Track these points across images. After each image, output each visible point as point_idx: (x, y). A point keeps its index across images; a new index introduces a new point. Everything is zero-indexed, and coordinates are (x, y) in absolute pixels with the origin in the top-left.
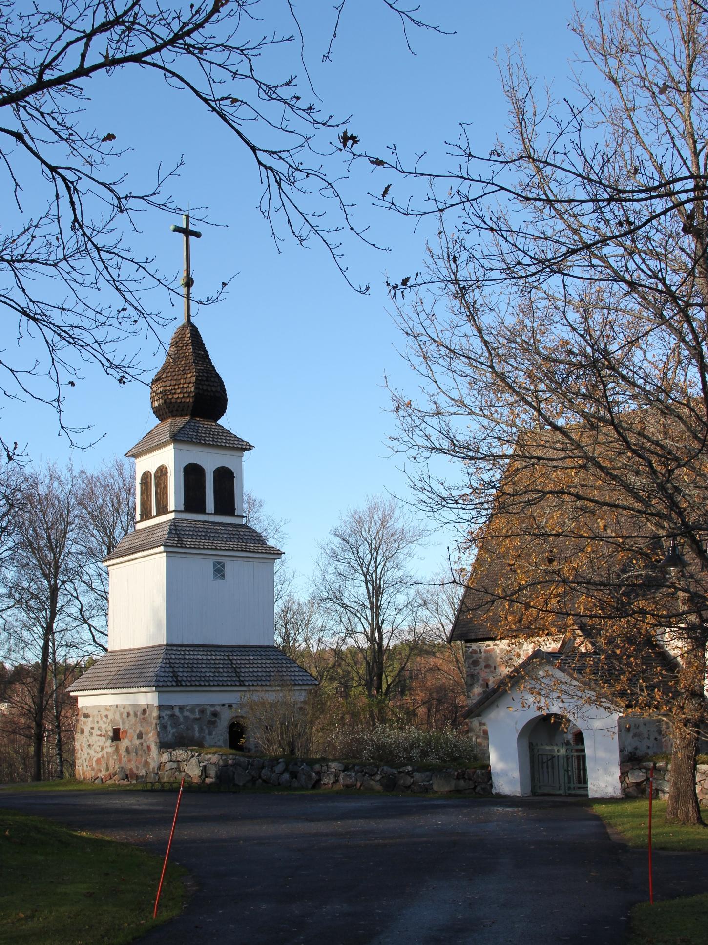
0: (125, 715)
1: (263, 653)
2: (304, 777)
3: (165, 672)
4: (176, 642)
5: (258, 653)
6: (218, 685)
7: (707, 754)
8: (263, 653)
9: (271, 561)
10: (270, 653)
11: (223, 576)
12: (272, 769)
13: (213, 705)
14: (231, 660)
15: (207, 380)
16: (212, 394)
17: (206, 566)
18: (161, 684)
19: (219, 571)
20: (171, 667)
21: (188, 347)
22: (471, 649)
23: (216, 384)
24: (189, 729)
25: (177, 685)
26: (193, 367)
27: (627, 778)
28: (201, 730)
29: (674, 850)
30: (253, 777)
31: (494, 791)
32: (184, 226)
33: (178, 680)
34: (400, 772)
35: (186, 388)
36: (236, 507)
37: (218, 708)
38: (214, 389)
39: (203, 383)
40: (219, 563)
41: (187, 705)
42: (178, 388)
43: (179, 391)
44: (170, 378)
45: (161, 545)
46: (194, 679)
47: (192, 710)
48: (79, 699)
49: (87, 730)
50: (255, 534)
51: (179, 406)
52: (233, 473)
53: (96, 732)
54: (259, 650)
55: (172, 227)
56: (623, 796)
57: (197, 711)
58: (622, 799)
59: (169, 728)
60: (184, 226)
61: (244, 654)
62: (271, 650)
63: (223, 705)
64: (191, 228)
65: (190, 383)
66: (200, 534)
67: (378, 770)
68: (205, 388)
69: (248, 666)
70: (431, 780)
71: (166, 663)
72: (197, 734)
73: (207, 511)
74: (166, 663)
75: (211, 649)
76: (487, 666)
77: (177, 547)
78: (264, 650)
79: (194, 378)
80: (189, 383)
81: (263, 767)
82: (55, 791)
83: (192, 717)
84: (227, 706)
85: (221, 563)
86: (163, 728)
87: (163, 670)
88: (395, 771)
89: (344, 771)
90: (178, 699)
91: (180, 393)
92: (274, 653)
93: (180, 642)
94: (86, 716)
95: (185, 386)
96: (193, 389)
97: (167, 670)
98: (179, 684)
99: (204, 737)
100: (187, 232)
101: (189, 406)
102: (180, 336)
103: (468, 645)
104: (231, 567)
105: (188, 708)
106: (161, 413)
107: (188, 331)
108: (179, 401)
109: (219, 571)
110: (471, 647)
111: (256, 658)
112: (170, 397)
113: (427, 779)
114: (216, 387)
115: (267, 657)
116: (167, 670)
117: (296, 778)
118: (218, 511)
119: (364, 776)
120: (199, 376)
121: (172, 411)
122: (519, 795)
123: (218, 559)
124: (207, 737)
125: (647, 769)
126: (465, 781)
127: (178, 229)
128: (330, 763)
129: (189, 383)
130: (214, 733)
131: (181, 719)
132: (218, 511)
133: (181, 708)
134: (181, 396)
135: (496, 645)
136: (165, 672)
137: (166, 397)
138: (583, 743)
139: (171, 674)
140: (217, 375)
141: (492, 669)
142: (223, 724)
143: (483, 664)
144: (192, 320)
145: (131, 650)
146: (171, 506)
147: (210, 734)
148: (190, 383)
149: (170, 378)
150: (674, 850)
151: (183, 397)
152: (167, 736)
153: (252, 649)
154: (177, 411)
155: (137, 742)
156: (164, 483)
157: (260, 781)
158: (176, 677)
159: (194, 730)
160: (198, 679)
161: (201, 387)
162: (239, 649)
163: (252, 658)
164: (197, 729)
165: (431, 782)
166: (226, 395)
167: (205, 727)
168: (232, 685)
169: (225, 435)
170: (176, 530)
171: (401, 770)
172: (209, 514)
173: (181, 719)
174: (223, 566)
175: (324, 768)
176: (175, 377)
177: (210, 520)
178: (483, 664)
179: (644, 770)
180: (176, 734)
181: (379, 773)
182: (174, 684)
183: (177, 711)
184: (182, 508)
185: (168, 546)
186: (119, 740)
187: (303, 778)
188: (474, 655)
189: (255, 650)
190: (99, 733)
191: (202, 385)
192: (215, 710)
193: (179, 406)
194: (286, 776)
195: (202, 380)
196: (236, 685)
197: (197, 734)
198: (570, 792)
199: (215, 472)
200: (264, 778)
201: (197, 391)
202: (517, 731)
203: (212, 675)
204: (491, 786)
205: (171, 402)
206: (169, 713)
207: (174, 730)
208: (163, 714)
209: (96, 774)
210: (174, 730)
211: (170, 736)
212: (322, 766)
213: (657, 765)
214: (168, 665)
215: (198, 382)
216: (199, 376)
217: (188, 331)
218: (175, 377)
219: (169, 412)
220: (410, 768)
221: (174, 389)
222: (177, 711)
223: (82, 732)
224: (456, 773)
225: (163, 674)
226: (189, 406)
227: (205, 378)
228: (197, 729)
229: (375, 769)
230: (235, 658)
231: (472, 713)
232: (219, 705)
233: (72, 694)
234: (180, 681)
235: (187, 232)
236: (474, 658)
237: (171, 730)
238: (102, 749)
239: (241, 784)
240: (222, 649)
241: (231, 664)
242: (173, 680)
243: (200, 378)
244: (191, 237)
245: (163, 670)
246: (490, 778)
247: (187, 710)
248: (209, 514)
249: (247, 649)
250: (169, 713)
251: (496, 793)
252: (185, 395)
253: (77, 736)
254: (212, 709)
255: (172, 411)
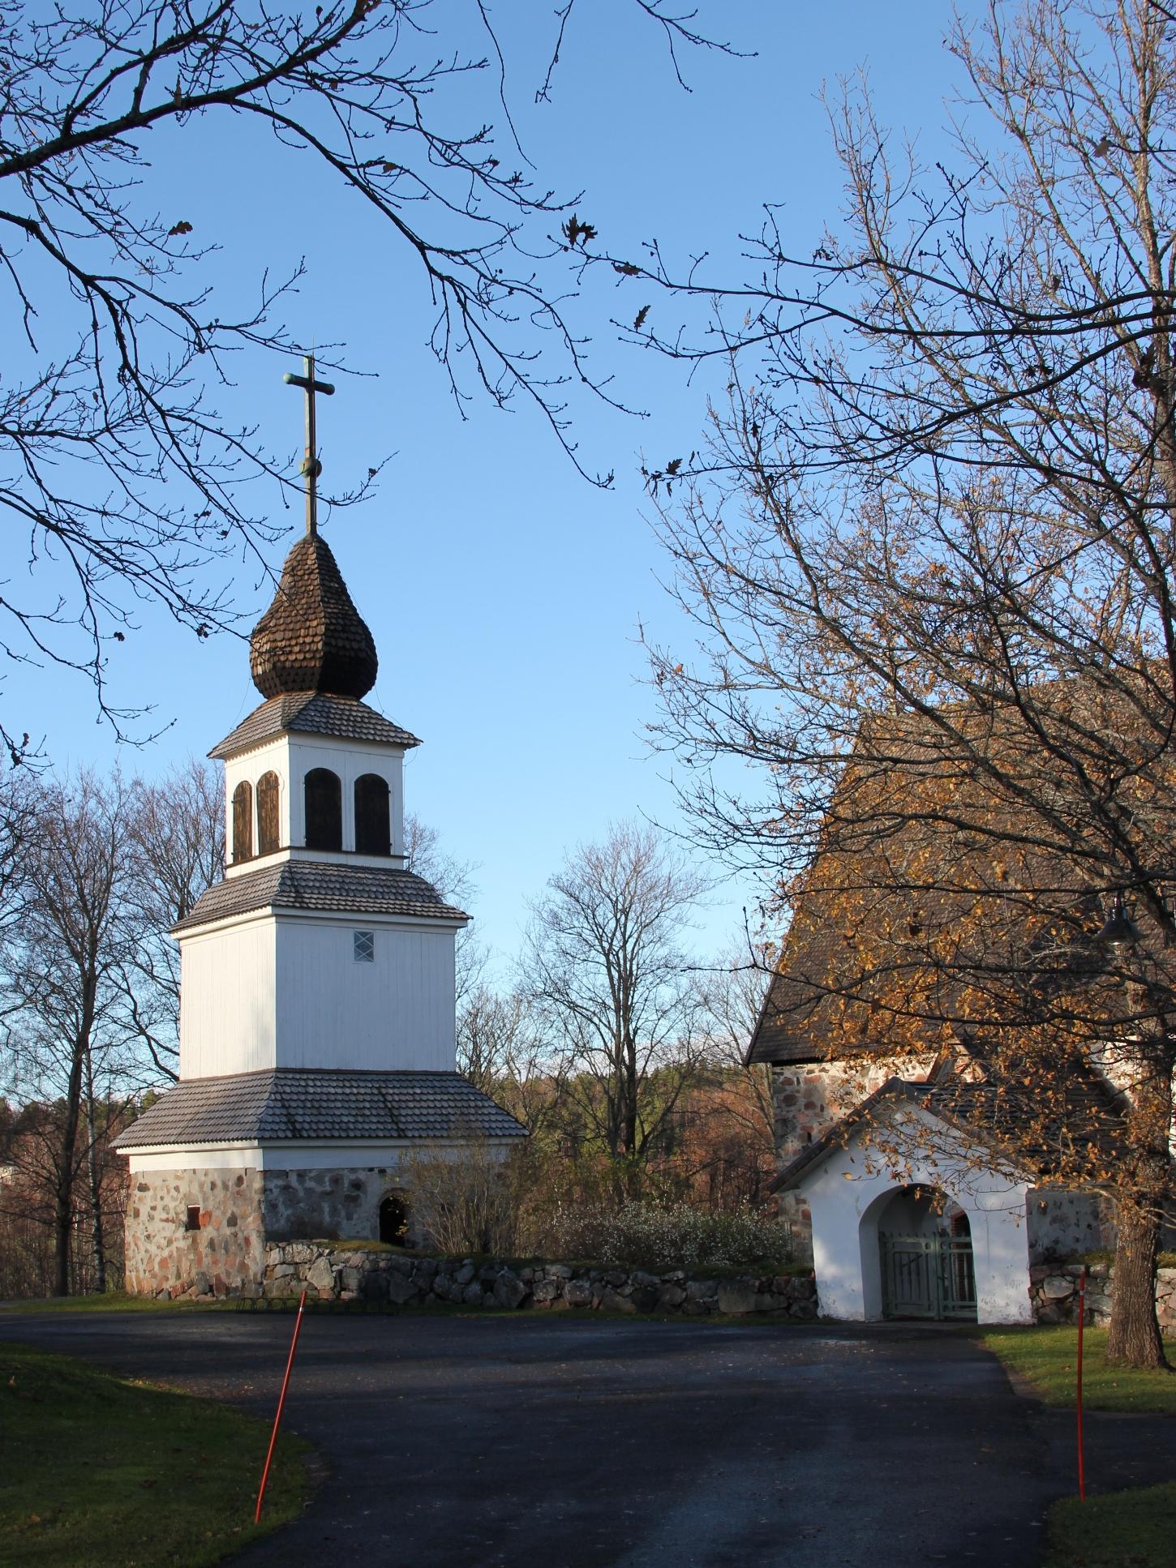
0: (207, 1187)
1: (437, 1084)
2: (505, 1289)
3: (274, 1114)
4: (292, 1065)
5: (429, 1084)
6: (363, 1137)
7: (1174, 1251)
8: (437, 1084)
9: (451, 931)
10: (449, 1083)
11: (371, 955)
12: (452, 1275)
13: (353, 1170)
14: (383, 1095)
15: (343, 631)
16: (353, 654)
17: (343, 939)
18: (267, 1135)
19: (364, 948)
20: (283, 1107)
21: (312, 577)
22: (782, 1078)
23: (358, 638)
24: (314, 1210)
25: (294, 1137)
26: (321, 608)
27: (1041, 1291)
28: (334, 1211)
29: (1119, 1411)
30: (421, 1290)
31: (820, 1313)
32: (306, 375)
33: (295, 1129)
34: (664, 1282)
35: (310, 644)
36: (392, 841)
37: (362, 1176)
38: (355, 645)
39: (336, 635)
40: (364, 934)
41: (310, 1171)
42: (296, 644)
43: (297, 649)
44: (282, 628)
45: (268, 904)
46: (322, 1126)
47: (319, 1179)
48: (132, 1159)
49: (144, 1211)
50: (423, 886)
51: (297, 674)
52: (386, 785)
53: (160, 1214)
54: (431, 1078)
55: (286, 377)
56: (1035, 1321)
57: (327, 1179)
58: (1033, 1325)
59: (281, 1208)
60: (306, 375)
61: (405, 1084)
62: (451, 1078)
63: (371, 1170)
64: (318, 378)
65: (315, 635)
66: (332, 886)
67: (628, 1278)
68: (340, 643)
69: (411, 1105)
70: (716, 1294)
71: (276, 1100)
72: (327, 1218)
73: (344, 848)
74: (276, 1100)
75: (350, 1077)
76: (810, 1105)
77: (294, 907)
78: (438, 1078)
79: (323, 627)
80: (314, 636)
81: (437, 1273)
82: (91, 1313)
83: (319, 1189)
84: (376, 1171)
85: (367, 934)
86: (270, 1207)
87: (271, 1112)
88: (656, 1280)
89: (571, 1279)
90: (296, 1160)
91: (300, 652)
92: (455, 1083)
93: (299, 1066)
94: (143, 1188)
95: (308, 640)
96: (320, 646)
97: (278, 1111)
98: (297, 1134)
99: (338, 1224)
100: (311, 386)
101: (313, 674)
102: (299, 558)
103: (778, 1069)
104: (384, 941)
105: (312, 1175)
106: (267, 685)
107: (311, 550)
108: (297, 665)
109: (364, 948)
110: (782, 1074)
111: (425, 1091)
112: (282, 658)
113: (709, 1293)
114: (359, 642)
115: (444, 1090)
116: (278, 1111)
117: (492, 1290)
118: (363, 848)
119: (605, 1287)
120: (331, 623)
121: (286, 683)
122: (863, 1319)
123: (363, 928)
124: (344, 1222)
125: (1075, 1276)
126: (772, 1297)
127: (295, 381)
128: (547, 1267)
129: (314, 636)
130: (355, 1216)
131: (301, 1194)
132: (363, 848)
133: (301, 1175)
134: (301, 657)
135: (823, 1070)
136: (274, 1114)
137: (276, 659)
138: (968, 1233)
139: (284, 1119)
140: (361, 622)
141: (818, 1110)
142: (371, 1201)
143: (802, 1102)
144: (320, 531)
145: (218, 1079)
146: (285, 840)
147: (349, 1217)
148: (315, 635)
149: (282, 628)
150: (1119, 1411)
151: (305, 658)
152: (278, 1221)
153: (419, 1077)
154: (294, 681)
155: (228, 1231)
156: (272, 801)
157: (432, 1295)
158: (293, 1123)
159: (322, 1212)
160: (329, 1126)
161: (333, 643)
162: (397, 1078)
163: (418, 1091)
164: (327, 1209)
165: (716, 1298)
166: (375, 656)
167: (340, 1206)
168: (385, 1137)
169: (373, 721)
170: (292, 879)
171: (666, 1278)
172: (347, 853)
173: (301, 1194)
174: (371, 940)
175: (537, 1274)
176: (291, 626)
177: (350, 863)
178: (802, 1102)
179: (1069, 1278)
180: (293, 1219)
181: (630, 1282)
182: (289, 1134)
183: (293, 1180)
184: (302, 842)
185: (280, 906)
186: (198, 1228)
187: (503, 1291)
188: (787, 1087)
189: (424, 1078)
190: (164, 1216)
191: (336, 639)
192: (357, 1178)
193: (297, 674)
194: (476, 1288)
195: (335, 630)
196: (392, 1137)
197: (327, 1218)
198: (947, 1314)
199: (357, 783)
200: (439, 1290)
201: (328, 649)
202: (859, 1212)
203: (352, 1119)
204: (816, 1304)
205: (284, 668)
206: (280, 1182)
207: (289, 1212)
208: (271, 1185)
209: (160, 1284)
210: (289, 1212)
211: (283, 1221)
212: (535, 1271)
213: (1092, 1269)
214: (279, 1104)
215: (330, 634)
216: (331, 623)
217: (311, 550)
218: (291, 626)
219: (281, 684)
220: (680, 1274)
221: (290, 646)
222: (293, 1180)
223: (137, 1214)
224: (757, 1283)
225: (270, 1119)
226: (313, 674)
227: (340, 628)
228: (327, 1209)
229: (624, 1277)
230: (391, 1091)
231: (784, 1183)
232: (364, 1169)
233: (119, 1152)
234: (299, 1130)
235: (311, 386)
236: (788, 1093)
237: (285, 1212)
238: (170, 1242)
239: (401, 1301)
240: (370, 1077)
241: (384, 1102)
242: (288, 1129)
243: (332, 628)
244: (317, 393)
245: (271, 1112)
246: (814, 1291)
247: (311, 1179)
248: (347, 853)
249: (410, 1078)
250: (280, 1182)
251: (824, 1316)
252: (308, 656)
253: (129, 1221)
254: (353, 1177)
255: (286, 683)
